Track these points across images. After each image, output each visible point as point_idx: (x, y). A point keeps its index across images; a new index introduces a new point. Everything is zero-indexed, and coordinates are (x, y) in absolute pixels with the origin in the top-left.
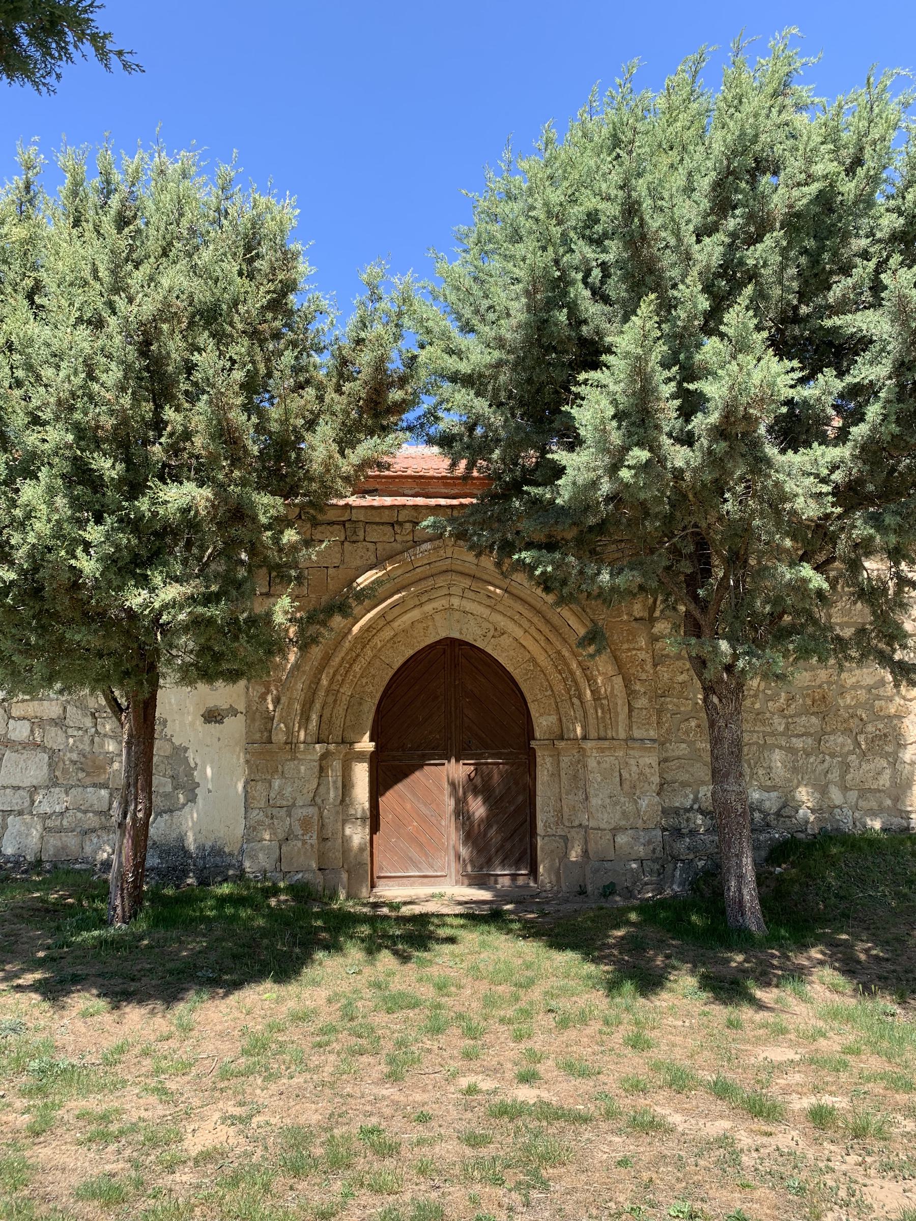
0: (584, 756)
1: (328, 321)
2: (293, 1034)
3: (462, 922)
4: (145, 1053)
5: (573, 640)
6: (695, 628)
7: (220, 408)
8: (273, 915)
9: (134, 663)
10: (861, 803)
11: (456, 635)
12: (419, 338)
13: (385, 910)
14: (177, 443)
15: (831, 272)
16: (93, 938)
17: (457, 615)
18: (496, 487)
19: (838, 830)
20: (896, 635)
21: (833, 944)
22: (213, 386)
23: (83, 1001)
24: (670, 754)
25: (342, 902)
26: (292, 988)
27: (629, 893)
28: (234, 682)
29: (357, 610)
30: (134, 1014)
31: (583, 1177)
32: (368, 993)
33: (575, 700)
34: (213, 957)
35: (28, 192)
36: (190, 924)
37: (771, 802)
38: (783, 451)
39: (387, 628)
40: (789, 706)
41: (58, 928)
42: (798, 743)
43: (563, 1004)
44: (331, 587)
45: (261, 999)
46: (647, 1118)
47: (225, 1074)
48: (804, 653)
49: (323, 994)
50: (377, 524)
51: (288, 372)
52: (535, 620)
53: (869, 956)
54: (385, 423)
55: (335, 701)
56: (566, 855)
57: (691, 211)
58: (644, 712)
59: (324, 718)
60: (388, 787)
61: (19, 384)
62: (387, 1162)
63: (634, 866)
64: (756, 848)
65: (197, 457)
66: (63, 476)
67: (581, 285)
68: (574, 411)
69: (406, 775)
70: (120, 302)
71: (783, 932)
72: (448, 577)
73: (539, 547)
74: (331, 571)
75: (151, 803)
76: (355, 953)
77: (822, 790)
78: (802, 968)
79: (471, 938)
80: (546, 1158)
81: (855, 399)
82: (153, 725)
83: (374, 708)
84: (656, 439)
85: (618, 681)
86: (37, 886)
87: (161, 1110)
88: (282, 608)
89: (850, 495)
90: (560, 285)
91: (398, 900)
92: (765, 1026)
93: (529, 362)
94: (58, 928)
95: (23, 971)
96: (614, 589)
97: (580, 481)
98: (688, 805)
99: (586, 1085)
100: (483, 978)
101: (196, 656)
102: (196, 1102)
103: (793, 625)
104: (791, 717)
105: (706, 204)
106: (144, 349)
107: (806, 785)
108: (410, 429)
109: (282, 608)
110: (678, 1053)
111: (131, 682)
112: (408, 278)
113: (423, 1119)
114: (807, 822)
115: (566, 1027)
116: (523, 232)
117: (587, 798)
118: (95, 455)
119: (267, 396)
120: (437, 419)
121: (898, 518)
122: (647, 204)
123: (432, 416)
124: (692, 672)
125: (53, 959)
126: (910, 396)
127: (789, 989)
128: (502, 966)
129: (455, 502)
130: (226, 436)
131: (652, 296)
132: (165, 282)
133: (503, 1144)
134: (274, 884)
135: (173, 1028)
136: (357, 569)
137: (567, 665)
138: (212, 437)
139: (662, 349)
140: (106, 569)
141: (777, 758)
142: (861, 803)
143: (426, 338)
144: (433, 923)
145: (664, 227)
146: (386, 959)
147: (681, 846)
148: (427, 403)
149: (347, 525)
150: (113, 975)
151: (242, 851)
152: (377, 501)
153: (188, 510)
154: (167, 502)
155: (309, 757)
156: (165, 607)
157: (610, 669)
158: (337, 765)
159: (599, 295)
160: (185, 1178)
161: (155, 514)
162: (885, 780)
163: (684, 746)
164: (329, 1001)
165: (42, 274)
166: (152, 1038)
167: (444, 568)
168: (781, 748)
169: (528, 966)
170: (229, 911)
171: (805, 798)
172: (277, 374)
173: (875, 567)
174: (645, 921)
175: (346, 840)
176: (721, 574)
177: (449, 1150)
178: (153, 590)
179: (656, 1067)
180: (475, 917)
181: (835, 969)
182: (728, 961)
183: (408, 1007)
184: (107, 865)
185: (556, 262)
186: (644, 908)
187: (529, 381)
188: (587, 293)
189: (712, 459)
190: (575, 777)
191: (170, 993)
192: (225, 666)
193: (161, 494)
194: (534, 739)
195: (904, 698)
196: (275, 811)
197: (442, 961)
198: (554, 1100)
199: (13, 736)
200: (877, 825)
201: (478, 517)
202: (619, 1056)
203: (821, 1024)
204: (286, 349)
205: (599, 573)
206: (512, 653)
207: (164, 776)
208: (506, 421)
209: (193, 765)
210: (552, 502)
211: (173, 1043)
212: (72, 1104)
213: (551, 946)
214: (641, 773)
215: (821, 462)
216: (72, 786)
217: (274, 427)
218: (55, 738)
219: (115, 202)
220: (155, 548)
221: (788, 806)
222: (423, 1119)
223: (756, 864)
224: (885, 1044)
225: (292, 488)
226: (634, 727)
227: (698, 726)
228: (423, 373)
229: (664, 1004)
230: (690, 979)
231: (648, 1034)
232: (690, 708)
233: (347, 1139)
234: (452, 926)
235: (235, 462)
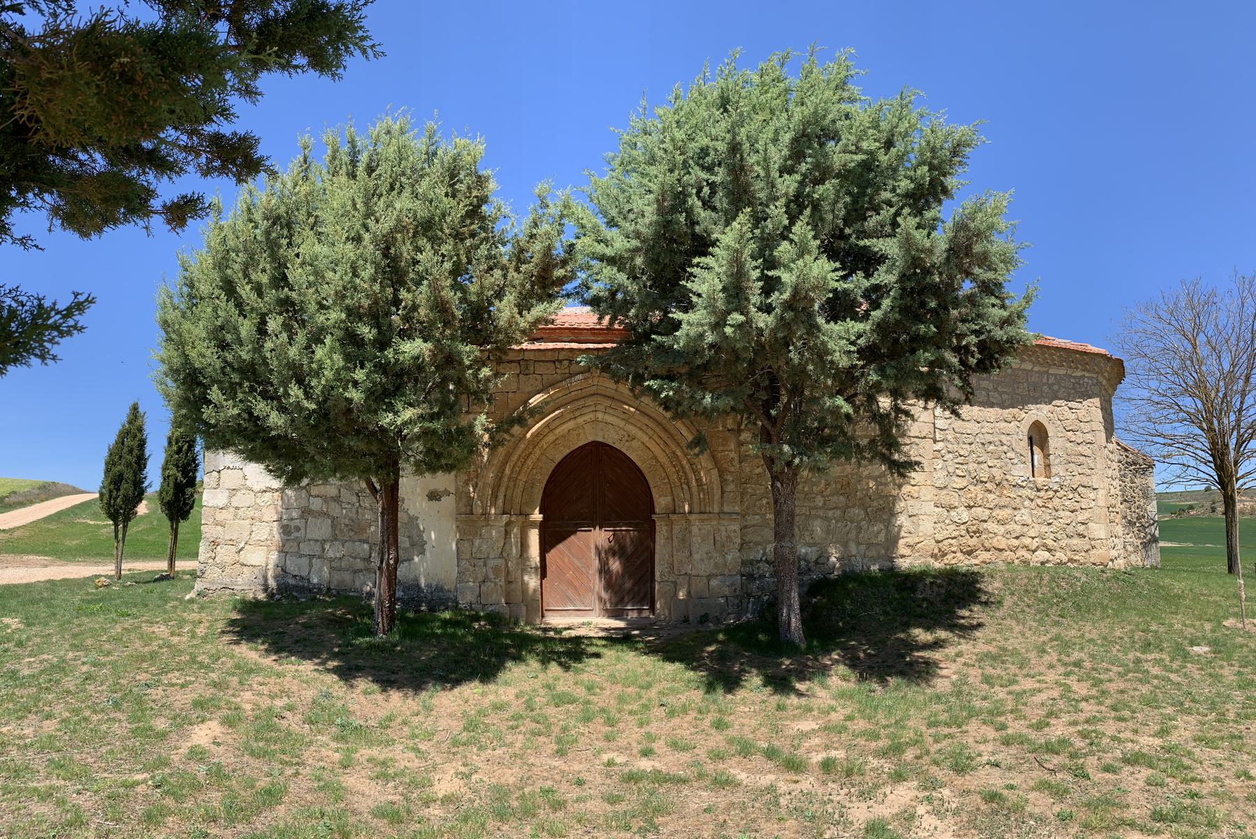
2: (493, 719)
4: (405, 723)
5: (684, 444)
7: (435, 288)
11: (601, 440)
13: (552, 634)
17: (601, 425)
23: (363, 684)
26: (492, 687)
27: (718, 621)
29: (530, 421)
30: (395, 696)
31: (682, 822)
32: (542, 692)
34: (442, 661)
36: (426, 638)
38: (828, 322)
43: (670, 700)
45: (472, 690)
46: (724, 778)
47: (456, 743)
48: (836, 454)
49: (512, 691)
52: (657, 429)
56: (676, 594)
57: (777, 156)
60: (551, 548)
62: (558, 814)
65: (421, 323)
68: (689, 285)
69: (564, 539)
73: (662, 378)
74: (510, 395)
76: (534, 664)
77: (845, 545)
79: (610, 654)
80: (658, 811)
84: (746, 307)
85: (715, 472)
86: (328, 605)
87: (417, 763)
88: (481, 422)
89: (869, 354)
96: (714, 409)
97: (692, 333)
99: (686, 757)
102: (438, 760)
105: (786, 152)
106: (386, 255)
109: (481, 422)
112: (568, 191)
113: (580, 783)
120: (589, 288)
122: (746, 146)
128: (630, 674)
130: (441, 307)
131: (749, 210)
132: (398, 206)
133: (631, 802)
138: (431, 310)
139: (752, 246)
140: (367, 398)
145: (758, 163)
146: (554, 668)
147: (753, 587)
148: (582, 275)
152: (543, 346)
153: (418, 358)
156: (405, 424)
157: (710, 465)
159: (707, 205)
160: (436, 812)
162: (882, 537)
164: (517, 697)
165: (318, 213)
169: (648, 673)
170: (450, 630)
172: (474, 262)
175: (524, 585)
177: (596, 806)
178: (396, 413)
179: (731, 742)
182: (782, 663)
186: (728, 631)
188: (700, 204)
192: (443, 462)
196: (476, 561)
197: (590, 670)
198: (664, 769)
199: (312, 507)
211: (421, 718)
212: (363, 752)
214: (728, 537)
217: (474, 298)
218: (335, 510)
222: (580, 783)
231: (727, 719)
233: (532, 794)
235: (447, 324)
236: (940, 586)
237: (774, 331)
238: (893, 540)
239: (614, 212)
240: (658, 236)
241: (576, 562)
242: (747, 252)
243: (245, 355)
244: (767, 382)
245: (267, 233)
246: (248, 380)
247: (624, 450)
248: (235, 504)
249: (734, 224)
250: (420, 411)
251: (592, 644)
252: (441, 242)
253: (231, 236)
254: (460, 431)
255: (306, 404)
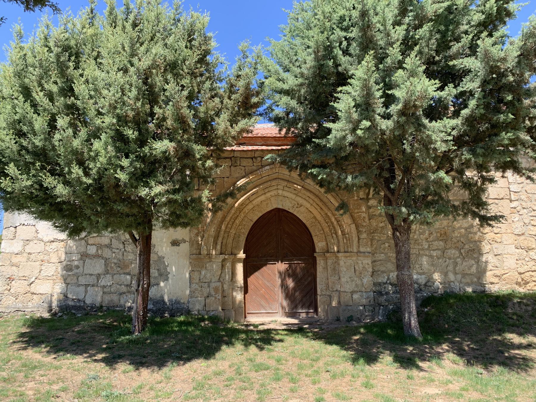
0: (338, 260)
1: (224, 68)
2: (215, 381)
3: (286, 332)
4: (151, 389)
5: (333, 208)
6: (388, 202)
7: (177, 108)
8: (203, 330)
9: (142, 220)
10: (463, 280)
12: (265, 74)
14: (159, 123)
15: (451, 41)
16: (126, 339)
18: (300, 140)
19: (452, 292)
20: (482, 204)
21: (452, 342)
22: (174, 98)
23: (123, 366)
24: (377, 259)
25: (233, 325)
26: (212, 361)
27: (359, 320)
28: (186, 228)
29: (238, 196)
30: (145, 372)
32: (246, 363)
33: (334, 235)
34: (178, 347)
35: (92, 14)
36: (167, 334)
37: (422, 279)
38: (430, 121)
39: (250, 204)
40: (430, 237)
41: (111, 335)
42: (434, 254)
44: (225, 186)
45: (198, 365)
48: (438, 213)
49: (227, 364)
50: (246, 158)
51: (208, 91)
52: (316, 200)
53: (469, 348)
54: (250, 112)
55: (228, 236)
56: (331, 303)
57: (391, 14)
58: (365, 240)
59: (223, 244)
60: (252, 273)
61: (91, 97)
63: (361, 308)
64: (417, 300)
65: (168, 129)
66: (112, 137)
67: (338, 48)
68: (336, 105)
70: (135, 60)
71: (429, 337)
72: (277, 181)
74: (225, 179)
75: (150, 281)
76: (239, 346)
77: (446, 274)
78: (439, 353)
79: (290, 340)
81: (463, 98)
82: (150, 247)
83: (245, 239)
84: (373, 116)
85: (353, 226)
89: (459, 141)
90: (329, 49)
91: (257, 323)
92: (424, 378)
93: (315, 84)
94: (111, 335)
95: (97, 353)
96: (353, 185)
97: (338, 136)
98: (385, 281)
100: (297, 357)
101: (169, 216)
103: (433, 200)
104: (431, 242)
105: (396, 12)
106: (145, 83)
107: (437, 272)
108: (261, 115)
110: (386, 390)
111: (141, 228)
112: (259, 47)
114: (438, 288)
115: (335, 378)
116: (312, 25)
117: (340, 278)
118: (125, 128)
119: (198, 101)
120: (272, 110)
121: (483, 150)
122: (371, 12)
123: (270, 109)
124: (387, 222)
125: (110, 348)
126: (489, 96)
127: (434, 362)
128: (305, 352)
129: (280, 148)
130: (181, 120)
131: (372, 52)
134: (203, 316)
135: (163, 378)
136: (237, 178)
137: (330, 219)
139: (376, 75)
140: (130, 178)
141: (425, 260)
142: (463, 280)
143: (268, 74)
144: (273, 334)
145: (379, 22)
146: (253, 348)
147: (382, 299)
149: (232, 159)
150: (135, 355)
151: (189, 302)
152: (245, 148)
153: (166, 152)
154: (156, 149)
155: (217, 261)
156: (156, 195)
158: (228, 265)
159: (346, 52)
161: (151, 154)
162: (474, 269)
163: (383, 255)
164: (230, 367)
165: (101, 50)
166: (154, 382)
167: (275, 177)
168: (426, 255)
170: (184, 328)
171: (437, 278)
172: (202, 92)
173: (470, 174)
174: (367, 332)
175: (233, 299)
176: (400, 178)
178: (151, 188)
180: (291, 330)
181: (454, 353)
182: (407, 349)
183: (265, 370)
184: (130, 308)
185: (328, 38)
187: (315, 92)
188: (341, 52)
189: (399, 125)
190: (334, 269)
191: (160, 363)
192: (182, 220)
193: (154, 145)
194: (315, 252)
195: (482, 233)
196: (203, 284)
197: (277, 347)
199: (89, 252)
200: (470, 290)
201: (291, 154)
202: (359, 391)
203: (449, 378)
204: (206, 80)
205: (346, 178)
206: (305, 214)
207: (154, 269)
208: (304, 110)
209: (167, 264)
210: (325, 146)
211: (163, 385)
213: (326, 343)
214: (364, 267)
215: (448, 126)
216: (115, 274)
217: (202, 115)
218: (107, 253)
219: (131, 17)
220: (151, 169)
221: (429, 282)
223: (417, 308)
224: (479, 387)
225: (209, 142)
226: (361, 247)
227: (389, 246)
228: (267, 89)
229: (378, 369)
230: (389, 358)
231: (371, 382)
232: (385, 238)
234: (282, 335)
235: (185, 131)
236: (527, 305)
237: (392, 131)
238: (482, 272)
239: (287, 62)
240: (315, 75)
241: (267, 283)
242: (372, 80)
243: (38, 142)
244: (388, 166)
245: (58, 56)
246: (39, 160)
247: (295, 213)
248: (28, 251)
249: (363, 62)
250: (166, 188)
251: (278, 334)
252: (183, 77)
253: (29, 54)
254: (193, 201)
255: (84, 179)
